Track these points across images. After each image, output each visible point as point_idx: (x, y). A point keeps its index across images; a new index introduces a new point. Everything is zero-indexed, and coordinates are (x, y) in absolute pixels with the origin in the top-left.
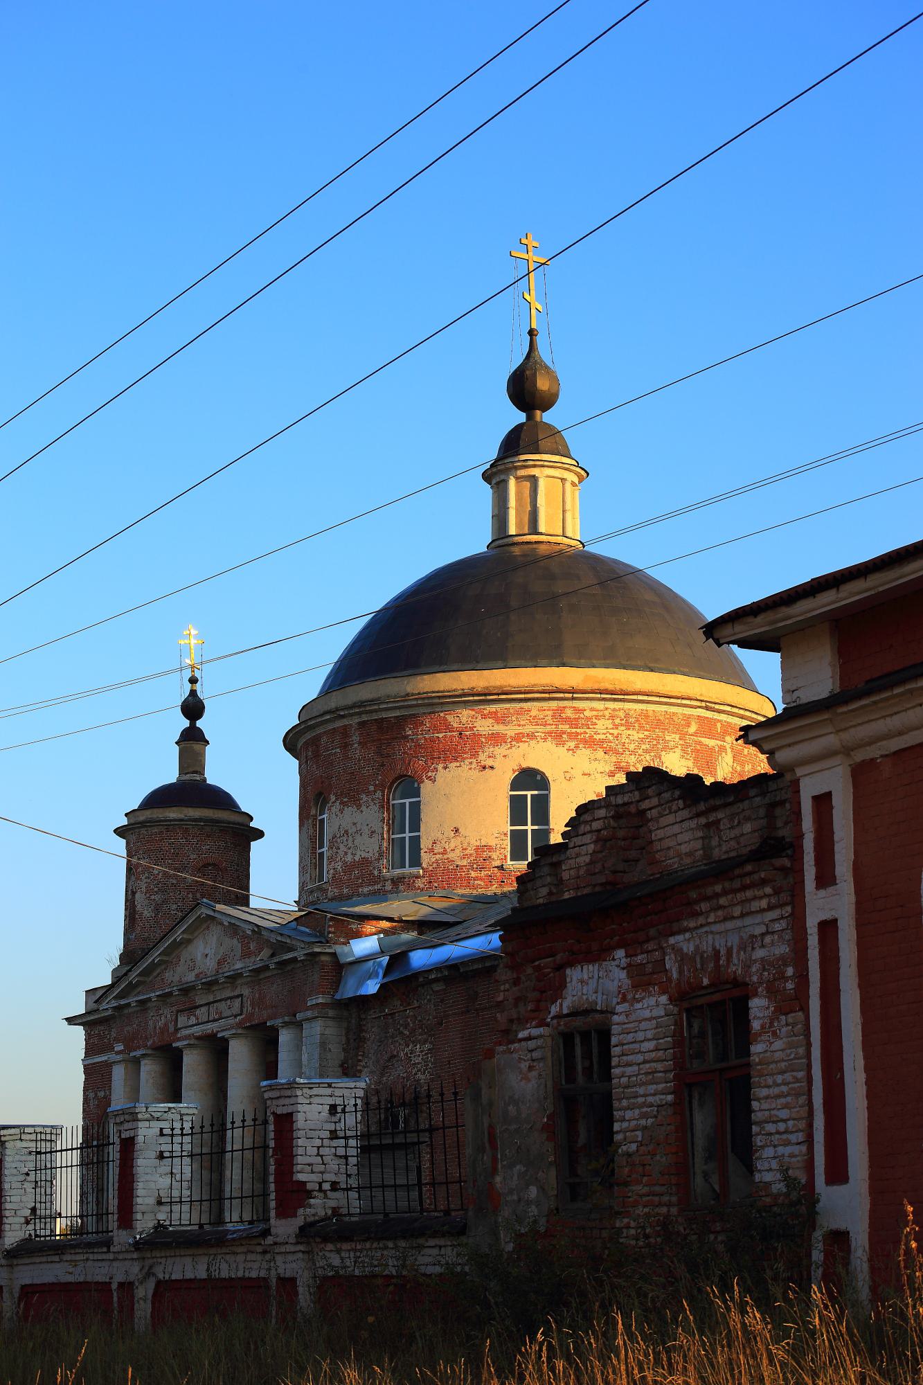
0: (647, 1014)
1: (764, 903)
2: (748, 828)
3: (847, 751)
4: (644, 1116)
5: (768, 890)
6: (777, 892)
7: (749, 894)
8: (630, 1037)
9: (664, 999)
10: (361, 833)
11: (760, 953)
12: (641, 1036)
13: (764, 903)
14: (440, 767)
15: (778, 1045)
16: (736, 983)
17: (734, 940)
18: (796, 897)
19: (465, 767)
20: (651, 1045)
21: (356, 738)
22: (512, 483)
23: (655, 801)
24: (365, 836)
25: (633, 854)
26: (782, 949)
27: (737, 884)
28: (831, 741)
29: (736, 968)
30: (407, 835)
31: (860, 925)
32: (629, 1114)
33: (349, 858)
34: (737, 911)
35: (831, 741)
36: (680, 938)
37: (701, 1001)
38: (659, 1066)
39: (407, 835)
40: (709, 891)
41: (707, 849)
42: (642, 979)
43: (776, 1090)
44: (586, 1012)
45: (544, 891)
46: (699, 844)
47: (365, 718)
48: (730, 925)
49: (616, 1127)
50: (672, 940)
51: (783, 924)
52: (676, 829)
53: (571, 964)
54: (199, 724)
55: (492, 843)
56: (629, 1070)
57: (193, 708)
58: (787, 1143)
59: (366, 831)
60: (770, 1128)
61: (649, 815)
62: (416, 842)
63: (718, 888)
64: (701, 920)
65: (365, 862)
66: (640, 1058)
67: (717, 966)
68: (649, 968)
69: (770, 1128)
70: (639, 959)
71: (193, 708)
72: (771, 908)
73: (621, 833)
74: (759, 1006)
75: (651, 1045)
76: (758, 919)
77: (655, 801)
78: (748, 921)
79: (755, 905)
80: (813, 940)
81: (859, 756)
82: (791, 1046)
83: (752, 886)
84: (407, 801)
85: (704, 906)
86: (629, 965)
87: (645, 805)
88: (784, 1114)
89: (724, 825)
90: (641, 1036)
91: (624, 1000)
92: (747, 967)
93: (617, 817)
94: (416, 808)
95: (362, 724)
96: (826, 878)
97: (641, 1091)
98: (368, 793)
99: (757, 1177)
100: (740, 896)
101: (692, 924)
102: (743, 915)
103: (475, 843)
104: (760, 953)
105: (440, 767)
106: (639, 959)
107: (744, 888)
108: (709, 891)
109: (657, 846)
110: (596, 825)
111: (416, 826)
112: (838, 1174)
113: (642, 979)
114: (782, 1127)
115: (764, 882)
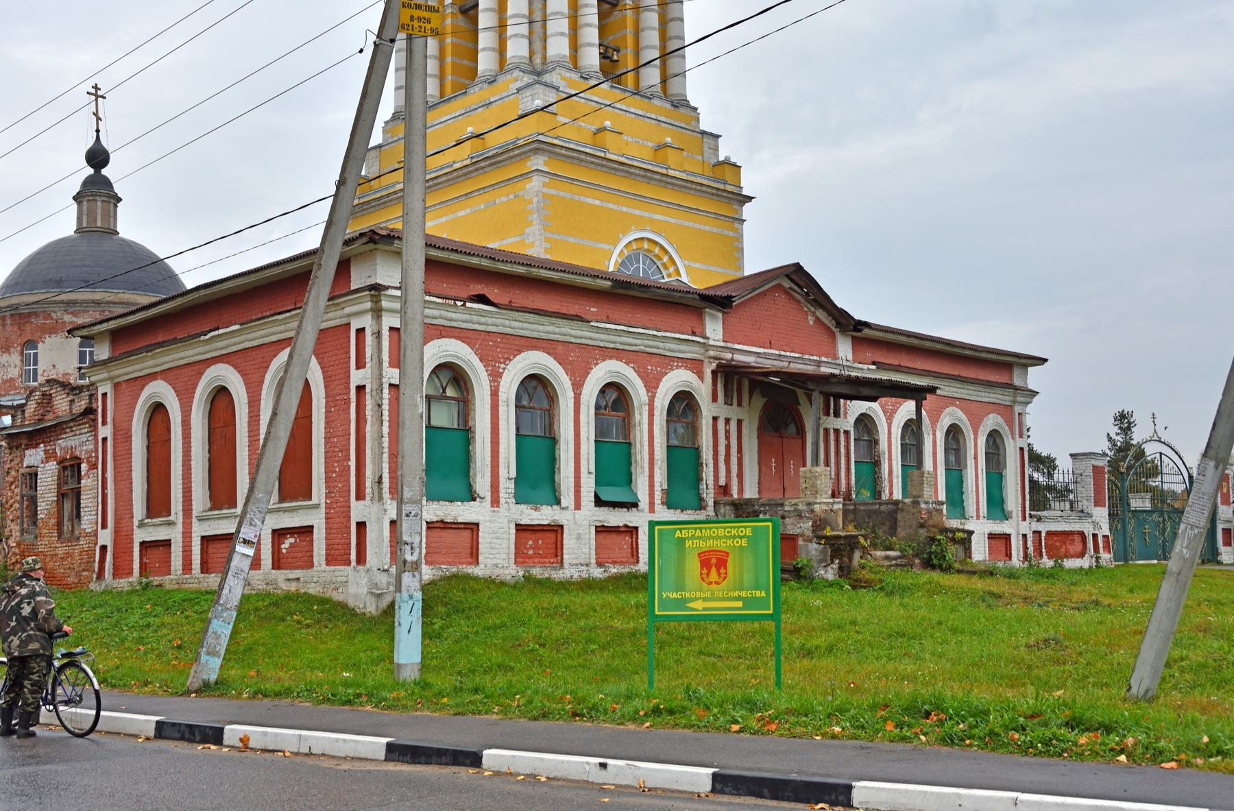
0: (49, 468)
1: (86, 430)
2: (83, 402)
3: (111, 379)
4: (47, 505)
5: (87, 426)
6: (90, 427)
7: (82, 427)
8: (44, 476)
9: (55, 463)
10: (10, 366)
11: (85, 448)
12: (47, 476)
13: (86, 430)
14: (47, 336)
15: (90, 480)
16: (77, 458)
17: (77, 443)
18: (95, 429)
19: (59, 336)
20: (50, 479)
21: (9, 322)
22: (85, 203)
23: (55, 390)
24: (12, 367)
25: (49, 409)
26: (92, 447)
27: (78, 423)
28: (105, 375)
29: (77, 453)
30: (32, 367)
31: (115, 439)
32: (42, 504)
33: (5, 378)
34: (78, 432)
35: (105, 375)
36: (60, 441)
37: (67, 464)
38: (52, 487)
39: (32, 367)
40: (69, 425)
41: (71, 409)
42: (49, 456)
43: (88, 496)
44: (31, 467)
45: (20, 420)
46: (68, 407)
47: (13, 312)
48: (76, 437)
49: (38, 509)
50: (59, 442)
51: (92, 438)
52: (61, 401)
53: (27, 449)
54: (104, 172)
55: (70, 372)
56: (43, 488)
57: (98, 157)
58: (91, 515)
59: (13, 366)
60: (86, 509)
61: (53, 395)
62: (35, 371)
63: (72, 424)
64: (67, 435)
65: (12, 379)
66: (46, 484)
67: (72, 452)
68: (51, 451)
69: (86, 509)
70: (48, 448)
71: (98, 157)
72: (88, 432)
73: (45, 401)
74: (84, 467)
75: (50, 479)
76: (84, 435)
77: (55, 390)
78: (82, 436)
79: (83, 431)
80: (100, 444)
81: (116, 380)
82: (93, 481)
83: (82, 424)
84: (32, 352)
85: (68, 430)
86: (45, 450)
87: (52, 392)
88: (90, 505)
89: (76, 401)
90: (47, 476)
91: (42, 463)
92: (81, 452)
93: (43, 395)
94: (36, 355)
95: (12, 315)
96: (104, 423)
97: (47, 496)
98: (14, 348)
99: (82, 527)
100: (79, 427)
101: (64, 436)
102: (80, 434)
103: (62, 372)
104: (85, 448)
105: (47, 336)
106: (48, 448)
107: (80, 425)
108: (69, 425)
109: (55, 407)
110: (37, 398)
111: (35, 363)
112: (104, 526)
113: (49, 456)
114: (89, 509)
115: (86, 423)
